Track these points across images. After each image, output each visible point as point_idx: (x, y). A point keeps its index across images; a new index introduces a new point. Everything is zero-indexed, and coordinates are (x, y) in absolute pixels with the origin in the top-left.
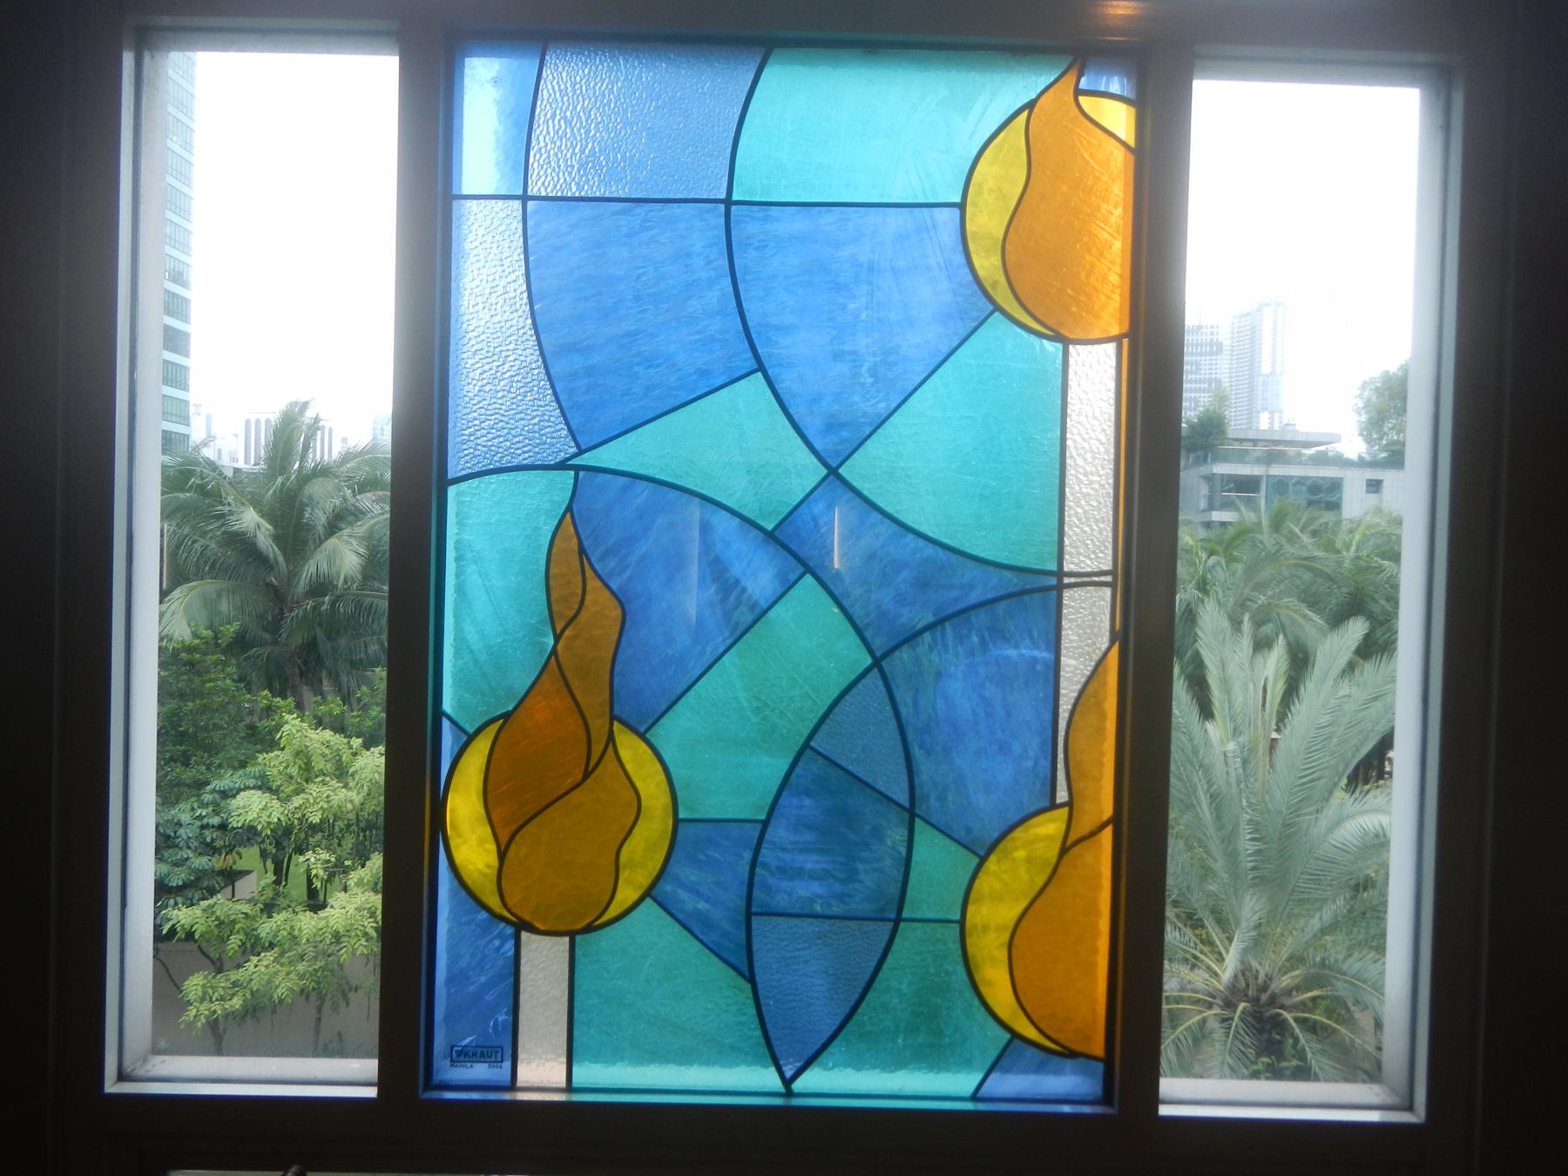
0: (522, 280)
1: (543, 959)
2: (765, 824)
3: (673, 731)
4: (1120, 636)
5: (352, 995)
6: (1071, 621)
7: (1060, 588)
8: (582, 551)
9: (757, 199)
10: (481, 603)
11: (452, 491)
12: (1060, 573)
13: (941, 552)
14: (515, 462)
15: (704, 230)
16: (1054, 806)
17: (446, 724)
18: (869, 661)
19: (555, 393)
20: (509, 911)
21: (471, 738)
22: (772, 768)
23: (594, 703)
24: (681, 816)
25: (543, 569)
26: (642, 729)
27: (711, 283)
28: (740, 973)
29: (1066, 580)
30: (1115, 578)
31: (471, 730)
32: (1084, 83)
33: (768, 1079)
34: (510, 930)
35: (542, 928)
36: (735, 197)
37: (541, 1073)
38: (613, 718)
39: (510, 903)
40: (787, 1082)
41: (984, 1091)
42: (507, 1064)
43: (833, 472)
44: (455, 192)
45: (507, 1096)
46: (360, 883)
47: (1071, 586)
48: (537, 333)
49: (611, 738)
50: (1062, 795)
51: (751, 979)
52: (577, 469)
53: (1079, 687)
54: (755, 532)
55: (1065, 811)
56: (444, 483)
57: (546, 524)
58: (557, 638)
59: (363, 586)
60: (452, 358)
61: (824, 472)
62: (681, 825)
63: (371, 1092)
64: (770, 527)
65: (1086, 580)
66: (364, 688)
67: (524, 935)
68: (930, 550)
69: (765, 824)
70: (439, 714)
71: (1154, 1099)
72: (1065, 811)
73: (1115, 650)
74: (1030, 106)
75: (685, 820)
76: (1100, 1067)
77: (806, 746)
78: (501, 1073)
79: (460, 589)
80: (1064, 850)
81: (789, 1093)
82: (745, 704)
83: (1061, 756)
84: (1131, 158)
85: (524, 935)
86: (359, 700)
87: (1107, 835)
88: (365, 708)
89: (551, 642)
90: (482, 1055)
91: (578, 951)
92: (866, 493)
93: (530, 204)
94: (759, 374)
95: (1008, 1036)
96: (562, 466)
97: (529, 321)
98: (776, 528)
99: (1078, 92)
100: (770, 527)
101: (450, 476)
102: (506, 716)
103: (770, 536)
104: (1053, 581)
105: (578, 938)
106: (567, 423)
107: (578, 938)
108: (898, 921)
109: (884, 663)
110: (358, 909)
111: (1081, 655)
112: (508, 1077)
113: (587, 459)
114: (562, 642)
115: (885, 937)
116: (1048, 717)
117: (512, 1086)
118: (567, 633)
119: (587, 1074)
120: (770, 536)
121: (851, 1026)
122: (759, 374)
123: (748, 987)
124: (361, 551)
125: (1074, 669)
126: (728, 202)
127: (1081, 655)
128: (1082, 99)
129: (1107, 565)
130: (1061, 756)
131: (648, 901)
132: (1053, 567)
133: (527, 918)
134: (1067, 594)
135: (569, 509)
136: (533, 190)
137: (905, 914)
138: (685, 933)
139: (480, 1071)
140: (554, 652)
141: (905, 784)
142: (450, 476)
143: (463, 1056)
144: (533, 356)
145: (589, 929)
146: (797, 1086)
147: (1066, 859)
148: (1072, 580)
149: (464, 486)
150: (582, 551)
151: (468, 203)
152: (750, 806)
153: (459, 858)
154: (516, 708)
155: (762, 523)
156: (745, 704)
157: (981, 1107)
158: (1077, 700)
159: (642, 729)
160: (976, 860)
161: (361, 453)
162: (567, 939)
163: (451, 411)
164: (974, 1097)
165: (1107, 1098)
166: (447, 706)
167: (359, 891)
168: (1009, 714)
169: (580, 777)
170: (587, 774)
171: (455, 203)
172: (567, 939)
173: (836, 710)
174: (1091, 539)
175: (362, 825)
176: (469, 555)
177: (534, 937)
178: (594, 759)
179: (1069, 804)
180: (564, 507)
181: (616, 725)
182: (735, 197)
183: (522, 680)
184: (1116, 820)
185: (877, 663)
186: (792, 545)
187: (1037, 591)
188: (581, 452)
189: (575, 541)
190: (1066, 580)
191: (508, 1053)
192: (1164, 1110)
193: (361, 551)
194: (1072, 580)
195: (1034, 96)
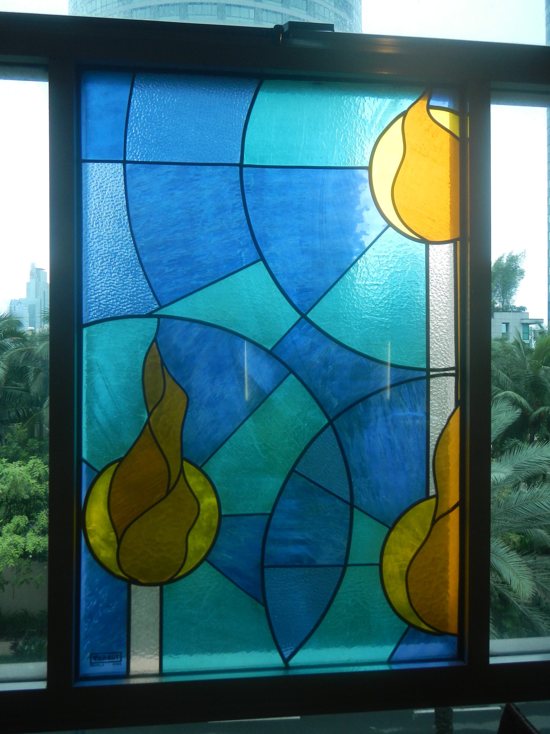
0: (125, 209)
1: (144, 602)
2: (271, 515)
3: (218, 465)
4: (460, 402)
5: (6, 587)
6: (434, 395)
7: (428, 378)
8: (163, 364)
9: (258, 164)
10: (104, 396)
11: (85, 331)
12: (428, 369)
13: (364, 360)
14: (123, 314)
15: (222, 183)
16: (428, 497)
17: (84, 466)
18: (326, 421)
19: (145, 274)
20: (124, 573)
21: (100, 474)
22: (272, 484)
23: (172, 451)
24: (223, 513)
25: (140, 374)
26: (200, 465)
27: (233, 210)
28: (260, 602)
29: (432, 373)
30: (457, 372)
31: (99, 469)
32: (433, 103)
33: (273, 658)
34: (125, 584)
35: (143, 581)
36: (245, 163)
37: (144, 664)
38: (183, 459)
39: (124, 568)
40: (286, 661)
41: (396, 656)
42: (124, 660)
43: (304, 316)
44: (83, 157)
45: (124, 682)
46: (8, 531)
47: (434, 376)
48: (134, 240)
49: (182, 471)
50: (432, 492)
51: (265, 604)
52: (159, 317)
53: (440, 431)
54: (262, 351)
55: (433, 501)
56: (81, 326)
57: (141, 349)
58: (150, 415)
59: (6, 384)
60: (84, 254)
61: (298, 316)
62: (223, 518)
63: (42, 685)
64: (269, 348)
65: (443, 373)
66: (9, 434)
67: (133, 587)
68: (359, 359)
69: (271, 515)
70: (80, 460)
71: (487, 654)
72: (433, 501)
73: (458, 410)
74: (404, 114)
75: (226, 516)
76: (455, 639)
77: (293, 470)
78: (122, 668)
79: (91, 387)
80: (434, 521)
81: (287, 667)
82: (258, 449)
83: (431, 470)
84: (458, 143)
85: (133, 587)
86: (6, 440)
87: (457, 511)
88: (10, 444)
89: (146, 417)
90: (109, 658)
91: (165, 595)
92: (322, 328)
93: (128, 165)
94: (261, 262)
95: (406, 626)
96: (150, 315)
97: (129, 233)
98: (273, 348)
99: (429, 107)
100: (269, 348)
101: (84, 322)
102: (121, 460)
103: (270, 353)
104: (424, 374)
105: (165, 587)
106: (153, 291)
107: (165, 587)
108: (345, 566)
109: (335, 423)
110: (10, 544)
111: (440, 414)
112: (125, 670)
113: (164, 312)
114: (152, 417)
115: (339, 576)
116: (424, 448)
117: (127, 675)
118: (155, 411)
119: (173, 663)
120: (270, 353)
121: (321, 626)
122: (261, 262)
123: (262, 608)
124: (5, 367)
125: (437, 422)
126: (241, 165)
127: (440, 414)
128: (432, 111)
129: (452, 364)
130: (431, 470)
131: (205, 563)
132: (424, 366)
133: (135, 577)
134: (432, 381)
135: (155, 340)
136: (129, 158)
137: (350, 562)
138: (227, 580)
139: (107, 667)
140: (148, 422)
141: (348, 490)
142: (84, 322)
143: (96, 657)
144: (130, 252)
145: (172, 580)
146: (292, 662)
147: (435, 527)
148: (434, 373)
149: (93, 327)
150: (163, 364)
151: (91, 165)
152: (261, 503)
153: (91, 541)
154: (126, 455)
155: (265, 346)
156: (258, 449)
157: (395, 667)
158: (439, 439)
159: (200, 465)
160: (387, 530)
161: (5, 318)
162: (158, 588)
163: (84, 284)
164: (389, 661)
165: (460, 655)
166: (85, 455)
167: (8, 535)
168: (403, 448)
169: (164, 494)
170: (168, 492)
171: (84, 165)
172: (158, 588)
173: (309, 449)
174: (444, 351)
175: (9, 501)
176: (97, 368)
177: (139, 588)
178: (171, 484)
179: (436, 496)
180: (152, 339)
181: (185, 463)
182: (245, 163)
183: (129, 439)
184: (461, 504)
185: (331, 422)
186: (280, 357)
187: (415, 379)
188: (161, 307)
189: (159, 358)
190: (432, 373)
191: (124, 654)
192: (493, 661)
193: (5, 367)
194: (434, 373)
195: (406, 109)
